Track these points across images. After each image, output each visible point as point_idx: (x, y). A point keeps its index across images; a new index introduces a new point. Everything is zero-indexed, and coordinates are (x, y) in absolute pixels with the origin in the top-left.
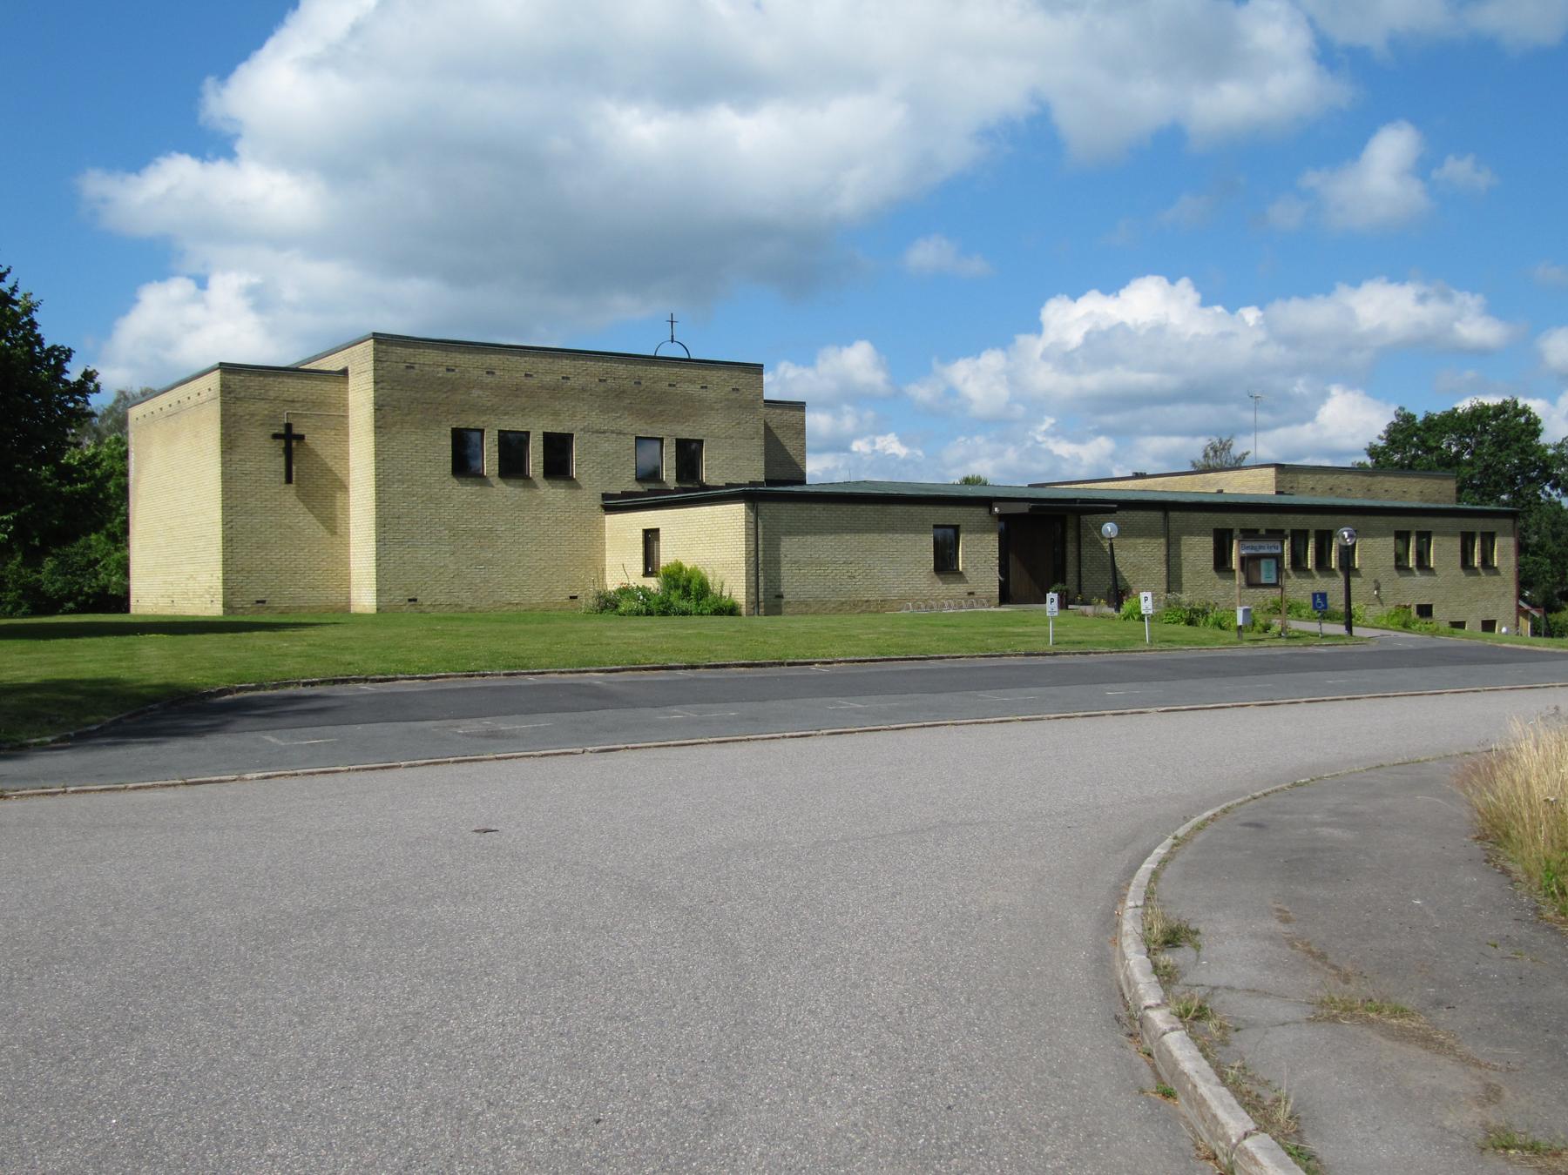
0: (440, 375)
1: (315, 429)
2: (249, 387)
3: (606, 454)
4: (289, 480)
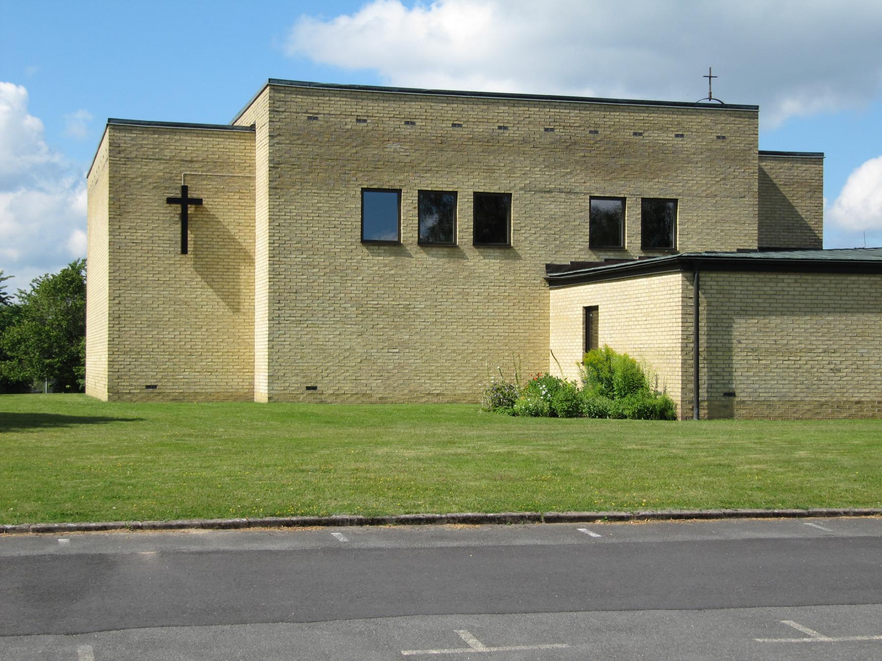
0: (349, 127)
1: (216, 193)
2: (142, 146)
3: (552, 218)
4: (184, 251)
